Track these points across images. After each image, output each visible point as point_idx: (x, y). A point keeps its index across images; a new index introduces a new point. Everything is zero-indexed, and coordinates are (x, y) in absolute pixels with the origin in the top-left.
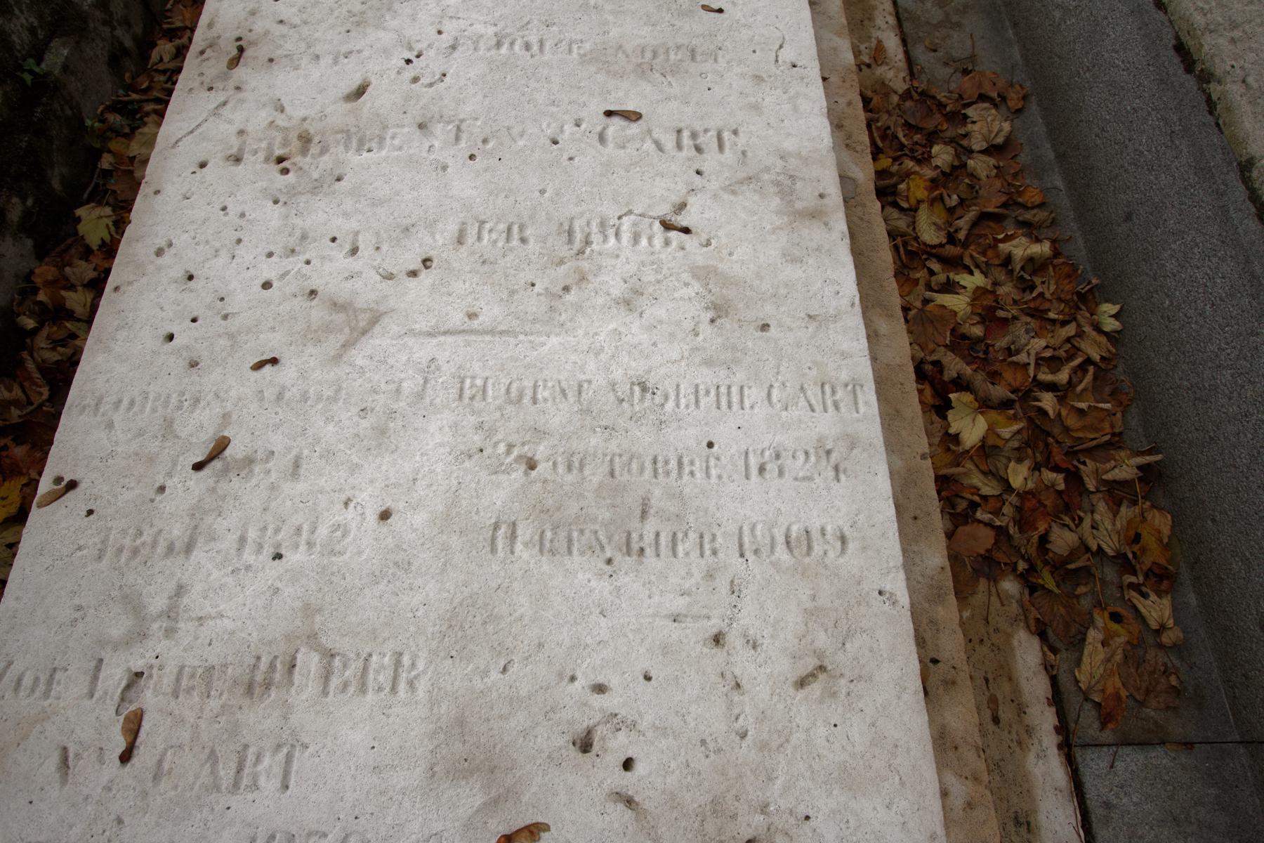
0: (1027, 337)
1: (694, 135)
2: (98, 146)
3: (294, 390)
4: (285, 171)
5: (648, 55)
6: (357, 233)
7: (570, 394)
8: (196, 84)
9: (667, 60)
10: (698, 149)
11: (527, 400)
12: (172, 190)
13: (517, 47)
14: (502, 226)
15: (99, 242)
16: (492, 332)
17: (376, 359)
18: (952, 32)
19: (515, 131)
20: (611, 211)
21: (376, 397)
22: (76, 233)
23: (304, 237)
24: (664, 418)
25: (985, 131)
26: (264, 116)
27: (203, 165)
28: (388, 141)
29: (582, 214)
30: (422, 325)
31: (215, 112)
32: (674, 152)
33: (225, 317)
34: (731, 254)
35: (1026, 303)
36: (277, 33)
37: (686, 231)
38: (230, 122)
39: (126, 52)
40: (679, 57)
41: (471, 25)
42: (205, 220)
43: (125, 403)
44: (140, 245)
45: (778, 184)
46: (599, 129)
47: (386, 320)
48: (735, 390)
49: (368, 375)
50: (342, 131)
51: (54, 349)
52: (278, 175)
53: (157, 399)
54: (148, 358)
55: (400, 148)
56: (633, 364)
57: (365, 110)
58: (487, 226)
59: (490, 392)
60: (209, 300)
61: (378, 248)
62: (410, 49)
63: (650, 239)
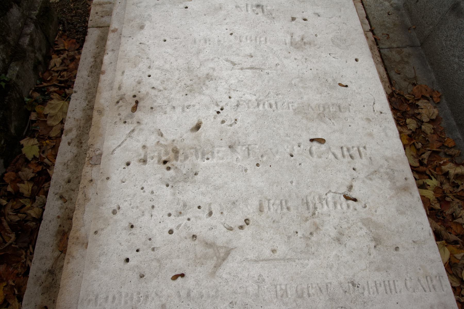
0: (459, 209)
1: (348, 150)
2: (29, 109)
3: (195, 291)
4: (169, 169)
5: (322, 109)
6: (210, 204)
7: (323, 291)
8: (118, 120)
9: (330, 111)
10: (351, 157)
11: (305, 295)
12: (115, 178)
13: (266, 106)
14: (278, 202)
15: (33, 157)
16: (284, 259)
17: (233, 274)
18: (405, 66)
19: (274, 151)
20: (323, 192)
21: (236, 296)
22: (21, 152)
23: (185, 205)
24: (365, 300)
25: (427, 113)
26: (153, 139)
27: (128, 164)
28: (216, 155)
29: (310, 193)
30: (251, 256)
31: (130, 135)
32: (342, 159)
33: (153, 249)
34: (376, 211)
35: (456, 193)
36: (153, 94)
37: (355, 200)
38: (138, 141)
39: (39, 63)
40: (334, 110)
41: (244, 95)
42: (135, 195)
43: (110, 299)
44: (104, 208)
45: (387, 174)
46: (309, 148)
47: (233, 253)
48: (391, 282)
49: (230, 283)
50: (193, 148)
51: (16, 215)
52: (166, 171)
53: (127, 295)
54: (118, 272)
55: (223, 159)
56: (347, 272)
57: (202, 137)
58: (272, 202)
59: (289, 292)
60: (143, 240)
61: (222, 213)
62: (217, 105)
63: (341, 205)
